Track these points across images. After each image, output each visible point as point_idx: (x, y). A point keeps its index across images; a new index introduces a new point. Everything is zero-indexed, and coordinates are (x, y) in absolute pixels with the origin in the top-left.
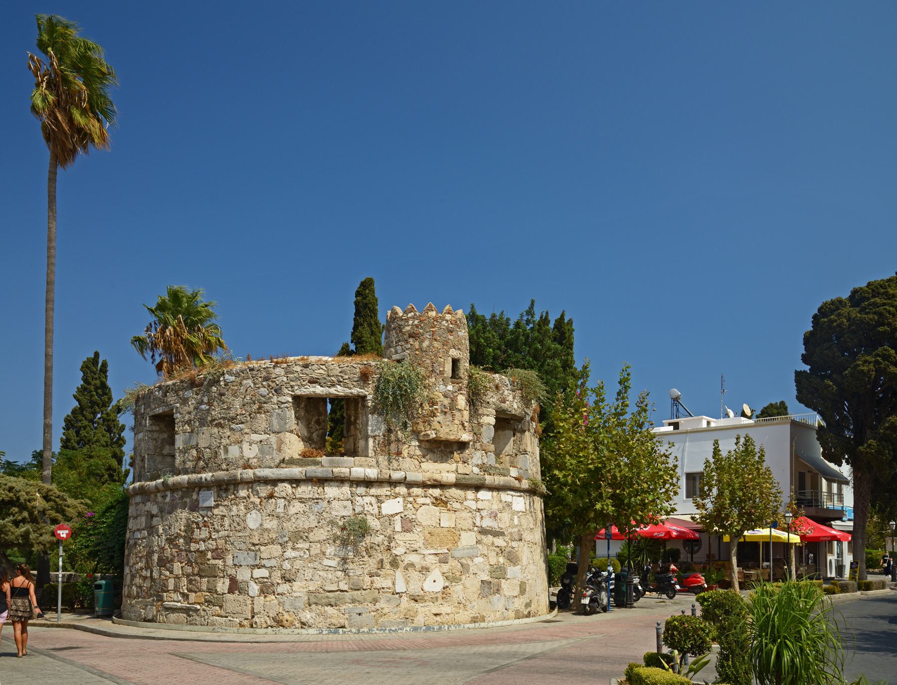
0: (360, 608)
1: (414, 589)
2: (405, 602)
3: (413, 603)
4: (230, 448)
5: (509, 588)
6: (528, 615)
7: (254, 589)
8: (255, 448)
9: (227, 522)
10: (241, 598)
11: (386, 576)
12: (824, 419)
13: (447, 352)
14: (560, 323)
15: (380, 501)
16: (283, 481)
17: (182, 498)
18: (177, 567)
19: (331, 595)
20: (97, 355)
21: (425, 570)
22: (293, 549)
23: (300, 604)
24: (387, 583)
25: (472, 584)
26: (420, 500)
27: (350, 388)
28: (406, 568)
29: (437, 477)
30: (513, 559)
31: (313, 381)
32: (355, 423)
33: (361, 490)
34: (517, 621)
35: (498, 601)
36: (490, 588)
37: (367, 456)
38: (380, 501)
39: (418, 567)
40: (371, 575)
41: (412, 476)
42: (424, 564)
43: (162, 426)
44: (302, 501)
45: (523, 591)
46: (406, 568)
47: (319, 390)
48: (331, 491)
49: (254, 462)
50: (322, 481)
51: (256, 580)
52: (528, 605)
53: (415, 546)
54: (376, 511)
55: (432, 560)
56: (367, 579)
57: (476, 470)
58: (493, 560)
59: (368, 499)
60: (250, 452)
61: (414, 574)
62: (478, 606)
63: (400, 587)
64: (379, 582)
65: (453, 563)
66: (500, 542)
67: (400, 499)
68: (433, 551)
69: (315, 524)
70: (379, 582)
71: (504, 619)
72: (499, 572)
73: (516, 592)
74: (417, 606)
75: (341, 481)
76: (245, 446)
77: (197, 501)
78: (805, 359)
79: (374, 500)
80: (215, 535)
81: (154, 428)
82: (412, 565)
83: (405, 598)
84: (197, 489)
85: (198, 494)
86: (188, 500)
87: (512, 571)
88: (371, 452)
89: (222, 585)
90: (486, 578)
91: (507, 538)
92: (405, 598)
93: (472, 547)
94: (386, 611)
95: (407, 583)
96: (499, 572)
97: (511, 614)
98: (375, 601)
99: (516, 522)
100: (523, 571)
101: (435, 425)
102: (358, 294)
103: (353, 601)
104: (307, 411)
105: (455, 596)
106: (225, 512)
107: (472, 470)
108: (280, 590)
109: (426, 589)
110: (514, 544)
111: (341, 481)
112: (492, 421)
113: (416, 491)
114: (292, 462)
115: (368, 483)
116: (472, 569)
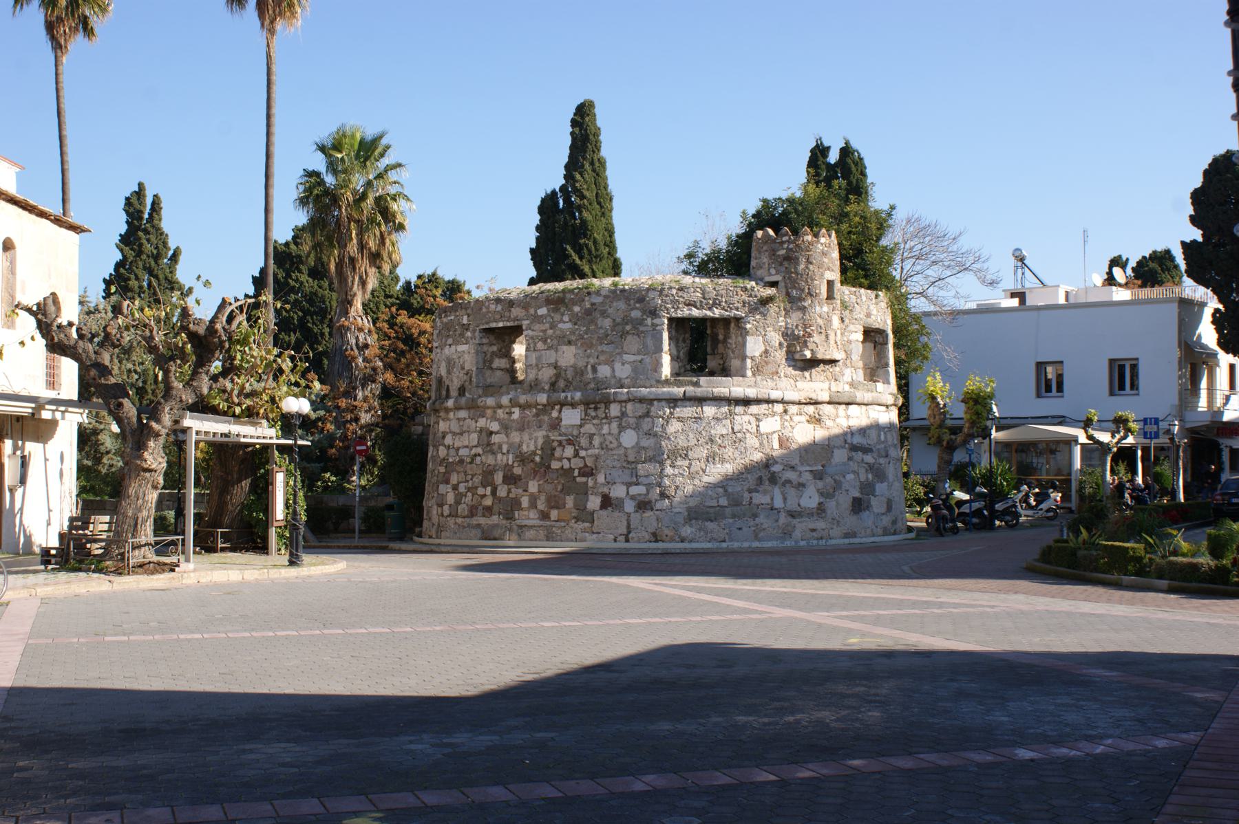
0: (739, 524)
1: (792, 504)
2: (783, 519)
3: (790, 519)
4: (599, 368)
5: (877, 505)
6: (895, 533)
7: (629, 506)
8: (628, 368)
9: (596, 441)
10: (616, 514)
11: (765, 492)
12: (1220, 301)
13: (822, 275)
14: (846, 151)
15: (758, 420)
16: (659, 400)
17: (537, 415)
18: (533, 487)
19: (712, 510)
20: (141, 185)
21: (801, 486)
22: (673, 466)
23: (680, 519)
24: (766, 499)
25: (845, 499)
26: (796, 419)
27: (581, 258)
28: (784, 484)
29: (814, 396)
30: (880, 475)
31: (689, 304)
32: (725, 341)
33: (739, 409)
34: (886, 538)
35: (867, 518)
36: (858, 506)
37: (744, 376)
38: (758, 420)
39: (795, 483)
40: (750, 491)
41: (791, 395)
42: (801, 480)
43: (492, 338)
44: (679, 419)
45: (889, 508)
46: (784, 484)
47: (696, 313)
48: (709, 411)
49: (627, 382)
50: (700, 401)
51: (633, 498)
52: (894, 522)
53: (793, 464)
54: (754, 430)
55: (807, 477)
56: (746, 495)
57: (847, 388)
58: (863, 478)
59: (746, 418)
60: (623, 371)
61: (791, 492)
62: (851, 521)
63: (778, 503)
64: (759, 498)
65: (829, 480)
66: (869, 458)
67: (778, 418)
68: (808, 468)
69: (694, 442)
70: (759, 498)
71: (874, 536)
72: (867, 488)
73: (883, 510)
74: (795, 521)
75: (718, 400)
76: (618, 366)
77: (559, 419)
78: (1194, 220)
79: (753, 420)
80: (582, 453)
81: (485, 341)
82: (789, 481)
83: (783, 514)
84: (557, 407)
85: (560, 412)
86: (546, 418)
87: (880, 488)
88: (749, 373)
89: (594, 502)
90: (857, 495)
91: (875, 455)
92: (783, 514)
93: (844, 464)
94: (765, 526)
95: (785, 499)
96: (867, 488)
97: (880, 531)
98: (755, 516)
99: (882, 438)
100: (890, 486)
101: (811, 345)
102: (574, 123)
103: (734, 516)
104: (677, 331)
105: (829, 512)
106: (593, 431)
107: (843, 387)
108: (658, 506)
109: (803, 504)
110: (882, 461)
111: (718, 400)
112: (861, 338)
113: (793, 409)
114: (667, 382)
115: (746, 402)
116: (845, 486)
